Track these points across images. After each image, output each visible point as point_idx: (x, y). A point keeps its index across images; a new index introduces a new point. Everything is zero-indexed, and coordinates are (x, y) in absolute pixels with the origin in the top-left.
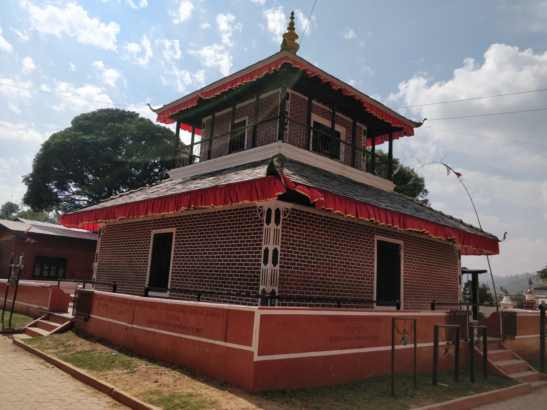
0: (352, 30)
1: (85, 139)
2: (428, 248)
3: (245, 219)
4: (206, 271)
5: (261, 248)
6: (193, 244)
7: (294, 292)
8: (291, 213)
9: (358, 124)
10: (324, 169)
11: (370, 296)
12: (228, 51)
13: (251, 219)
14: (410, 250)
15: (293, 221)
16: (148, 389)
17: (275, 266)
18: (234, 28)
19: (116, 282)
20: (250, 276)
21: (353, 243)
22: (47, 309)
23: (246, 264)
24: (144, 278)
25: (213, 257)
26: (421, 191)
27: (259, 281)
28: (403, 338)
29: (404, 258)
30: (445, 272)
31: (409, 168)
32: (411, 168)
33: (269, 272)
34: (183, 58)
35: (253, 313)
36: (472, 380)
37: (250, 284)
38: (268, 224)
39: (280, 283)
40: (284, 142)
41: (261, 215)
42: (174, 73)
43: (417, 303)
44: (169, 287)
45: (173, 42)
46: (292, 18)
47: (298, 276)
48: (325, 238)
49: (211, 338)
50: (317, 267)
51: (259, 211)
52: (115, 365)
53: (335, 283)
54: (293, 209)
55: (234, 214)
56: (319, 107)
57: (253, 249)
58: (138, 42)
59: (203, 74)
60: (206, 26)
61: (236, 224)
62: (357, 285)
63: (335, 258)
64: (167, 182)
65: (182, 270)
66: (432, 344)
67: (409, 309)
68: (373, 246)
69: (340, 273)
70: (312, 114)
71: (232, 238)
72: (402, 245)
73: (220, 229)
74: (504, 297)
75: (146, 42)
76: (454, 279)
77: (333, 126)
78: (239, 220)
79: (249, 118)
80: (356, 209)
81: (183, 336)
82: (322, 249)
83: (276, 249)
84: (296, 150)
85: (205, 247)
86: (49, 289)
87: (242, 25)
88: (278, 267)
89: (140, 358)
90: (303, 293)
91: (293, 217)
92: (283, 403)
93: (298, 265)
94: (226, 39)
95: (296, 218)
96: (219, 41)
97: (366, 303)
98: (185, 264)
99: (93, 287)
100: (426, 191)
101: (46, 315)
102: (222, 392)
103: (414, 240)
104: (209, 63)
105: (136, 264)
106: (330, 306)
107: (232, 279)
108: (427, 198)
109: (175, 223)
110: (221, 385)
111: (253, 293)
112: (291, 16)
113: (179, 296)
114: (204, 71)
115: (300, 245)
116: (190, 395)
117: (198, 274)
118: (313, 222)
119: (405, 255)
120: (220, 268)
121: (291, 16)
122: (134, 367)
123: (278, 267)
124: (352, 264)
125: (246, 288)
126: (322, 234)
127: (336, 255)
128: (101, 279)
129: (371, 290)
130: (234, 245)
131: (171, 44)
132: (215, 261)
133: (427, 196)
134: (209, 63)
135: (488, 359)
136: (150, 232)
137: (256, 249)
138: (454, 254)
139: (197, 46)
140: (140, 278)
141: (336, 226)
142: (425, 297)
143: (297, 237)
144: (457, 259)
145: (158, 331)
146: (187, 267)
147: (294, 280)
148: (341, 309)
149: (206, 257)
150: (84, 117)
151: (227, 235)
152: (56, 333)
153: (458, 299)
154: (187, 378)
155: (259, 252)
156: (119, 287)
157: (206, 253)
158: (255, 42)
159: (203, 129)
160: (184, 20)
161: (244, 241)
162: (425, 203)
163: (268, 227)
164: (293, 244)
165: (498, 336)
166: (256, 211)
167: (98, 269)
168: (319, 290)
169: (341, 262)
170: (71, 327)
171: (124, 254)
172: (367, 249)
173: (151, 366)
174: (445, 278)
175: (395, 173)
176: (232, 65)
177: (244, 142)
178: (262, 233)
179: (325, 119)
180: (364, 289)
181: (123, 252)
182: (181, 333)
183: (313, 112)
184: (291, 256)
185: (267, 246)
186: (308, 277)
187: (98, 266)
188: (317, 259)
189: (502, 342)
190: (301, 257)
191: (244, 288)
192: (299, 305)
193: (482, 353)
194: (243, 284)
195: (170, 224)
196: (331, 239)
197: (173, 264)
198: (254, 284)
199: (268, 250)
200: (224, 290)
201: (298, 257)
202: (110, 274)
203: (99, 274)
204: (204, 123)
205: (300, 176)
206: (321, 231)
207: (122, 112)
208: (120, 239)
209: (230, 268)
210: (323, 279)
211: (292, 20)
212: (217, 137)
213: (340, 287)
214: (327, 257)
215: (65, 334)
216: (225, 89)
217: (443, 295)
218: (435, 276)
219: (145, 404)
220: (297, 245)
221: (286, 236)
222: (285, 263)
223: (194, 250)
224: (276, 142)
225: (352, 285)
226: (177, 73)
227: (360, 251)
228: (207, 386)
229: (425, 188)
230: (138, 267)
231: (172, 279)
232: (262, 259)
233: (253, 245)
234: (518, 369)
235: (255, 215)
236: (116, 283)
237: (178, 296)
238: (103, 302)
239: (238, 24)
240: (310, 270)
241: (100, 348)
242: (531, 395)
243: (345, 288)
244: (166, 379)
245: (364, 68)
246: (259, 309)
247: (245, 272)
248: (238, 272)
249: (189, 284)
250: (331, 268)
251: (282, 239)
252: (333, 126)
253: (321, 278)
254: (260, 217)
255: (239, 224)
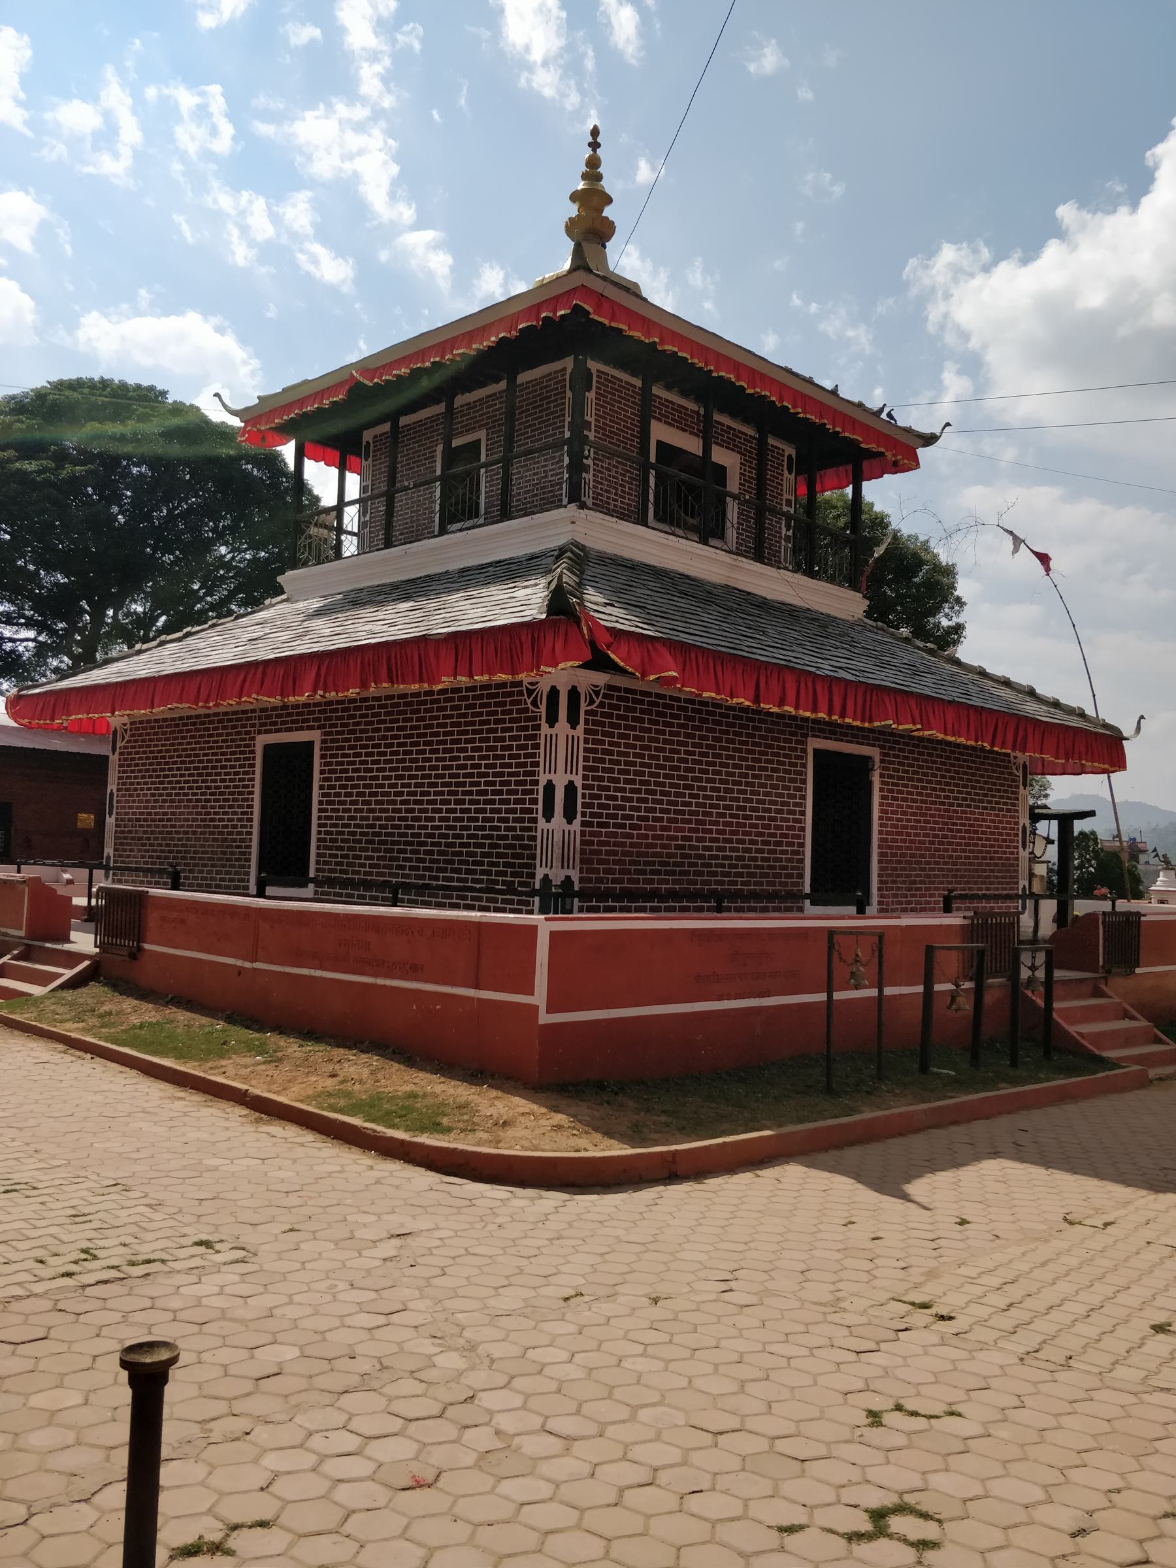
0: (773, 41)
1: (26, 473)
2: (942, 763)
3: (495, 713)
4: (405, 835)
5: (536, 783)
6: (367, 770)
7: (614, 881)
8: (605, 696)
9: (771, 441)
10: (686, 572)
11: (793, 884)
12: (382, 124)
13: (510, 712)
14: (897, 770)
15: (610, 716)
16: (319, 1089)
17: (570, 822)
18: (394, 41)
19: (178, 864)
20: (512, 846)
21: (754, 760)
22: (22, 933)
23: (501, 820)
24: (244, 853)
25: (420, 802)
26: (947, 601)
27: (534, 857)
28: (852, 973)
29: (881, 790)
30: (984, 820)
31: (917, 538)
32: (922, 538)
33: (558, 837)
34: (239, 148)
35: (533, 930)
36: (1014, 1064)
37: (512, 865)
38: (552, 726)
39: (582, 861)
40: (583, 506)
41: (535, 703)
42: (215, 201)
43: (913, 896)
44: (312, 874)
45: (202, 94)
46: (595, 145)
47: (623, 844)
48: (686, 753)
49: (445, 983)
50: (669, 820)
51: (530, 692)
52: (232, 1048)
53: (711, 857)
54: (610, 687)
55: (466, 698)
56: (671, 402)
57: (517, 783)
58: (92, 96)
59: (306, 206)
60: (306, 34)
61: (473, 723)
62: (763, 860)
63: (711, 798)
64: (281, 606)
65: (342, 833)
66: (920, 989)
67: (892, 910)
68: (804, 766)
69: (723, 832)
70: (653, 423)
71: (465, 758)
72: (877, 759)
73: (433, 734)
74: (1161, 874)
75: (115, 96)
76: (1008, 834)
77: (707, 450)
78: (480, 714)
79: (488, 434)
80: (758, 684)
81: (380, 981)
82: (680, 778)
83: (571, 783)
84: (615, 526)
85: (398, 777)
86: (21, 887)
87: (420, 30)
88: (577, 825)
89: (280, 1033)
90: (637, 881)
91: (611, 706)
92: (601, 1104)
93: (624, 817)
94: (370, 79)
95: (618, 708)
96: (348, 89)
97: (789, 901)
98: (351, 818)
99: (107, 877)
100: (958, 601)
101: (21, 948)
102: (474, 1089)
103: (908, 744)
104: (324, 167)
105: (221, 820)
106: (700, 909)
107: (469, 854)
108: (961, 620)
109: (317, 720)
110: (472, 1075)
111: (521, 884)
112: (590, 139)
113: (340, 895)
114: (308, 194)
115: (627, 772)
116: (412, 1095)
117: (384, 842)
118: (659, 714)
119: (883, 783)
120: (440, 828)
121: (590, 139)
122: (275, 1051)
123: (577, 825)
124: (752, 809)
125: (504, 874)
126: (679, 743)
127: (713, 789)
128: (129, 856)
129: (798, 868)
130: (471, 775)
131: (197, 100)
132: (425, 811)
133: (962, 614)
134: (324, 167)
135: (1055, 1015)
136: (253, 739)
137: (524, 783)
138: (1011, 774)
139: (281, 106)
140: (232, 853)
141: (715, 722)
142: (933, 883)
143: (620, 754)
144: (1017, 787)
145: (318, 973)
146: (357, 826)
147: (615, 853)
148: (724, 915)
149: (403, 802)
150: (12, 406)
151: (451, 751)
152: (62, 987)
153: (1017, 883)
154: (396, 1066)
155: (531, 792)
156: (186, 878)
157: (401, 794)
158: (465, 92)
159: (366, 460)
160: (233, 12)
161: (493, 766)
162: (957, 633)
163: (553, 731)
164: (612, 771)
165: (1092, 967)
166: (521, 693)
167: (116, 832)
168: (673, 873)
169: (726, 807)
170: (94, 973)
171: (186, 795)
172: (789, 772)
173: (309, 1047)
174: (984, 833)
175: (876, 555)
176: (395, 169)
177: (478, 504)
178: (537, 746)
179: (687, 434)
180: (782, 868)
181: (182, 788)
182: (376, 976)
183: (655, 418)
184: (608, 798)
185: (551, 777)
186: (648, 846)
187: (117, 826)
188: (669, 803)
189: (1103, 981)
190: (631, 800)
191: (498, 873)
192: (628, 910)
193: (1041, 1003)
194: (497, 865)
195: (304, 721)
196: (701, 754)
197: (320, 818)
198: (521, 866)
200: (451, 879)
201: (624, 799)
202: (151, 845)
203: (122, 844)
204: (368, 443)
205: (628, 605)
206: (678, 734)
207: (119, 387)
208: (171, 757)
209: (463, 828)
210: (682, 847)
211: (594, 151)
212: (407, 488)
213: (723, 866)
214: (691, 796)
215: (84, 990)
216: (423, 362)
217: (979, 877)
218: (959, 831)
219: (325, 1113)
220: (620, 772)
221: (595, 751)
222: (592, 815)
223: (369, 786)
224: (563, 510)
225: (751, 859)
226: (225, 201)
227: (770, 778)
228: (443, 1079)
229: (956, 593)
230: (226, 826)
231: (318, 855)
232: (540, 806)
233: (517, 774)
234: (1128, 1039)
235: (519, 702)
236: (179, 868)
237: (336, 894)
238: (175, 915)
239: (406, 28)
240: (653, 828)
241: (182, 1016)
242: (1142, 1093)
243: (736, 866)
244: (352, 1069)
245: (810, 177)
247: (500, 837)
248: (484, 837)
249: (363, 865)
250: (703, 822)
251: (586, 759)
252: (707, 450)
253: (678, 847)
254: (531, 708)
255: (482, 723)
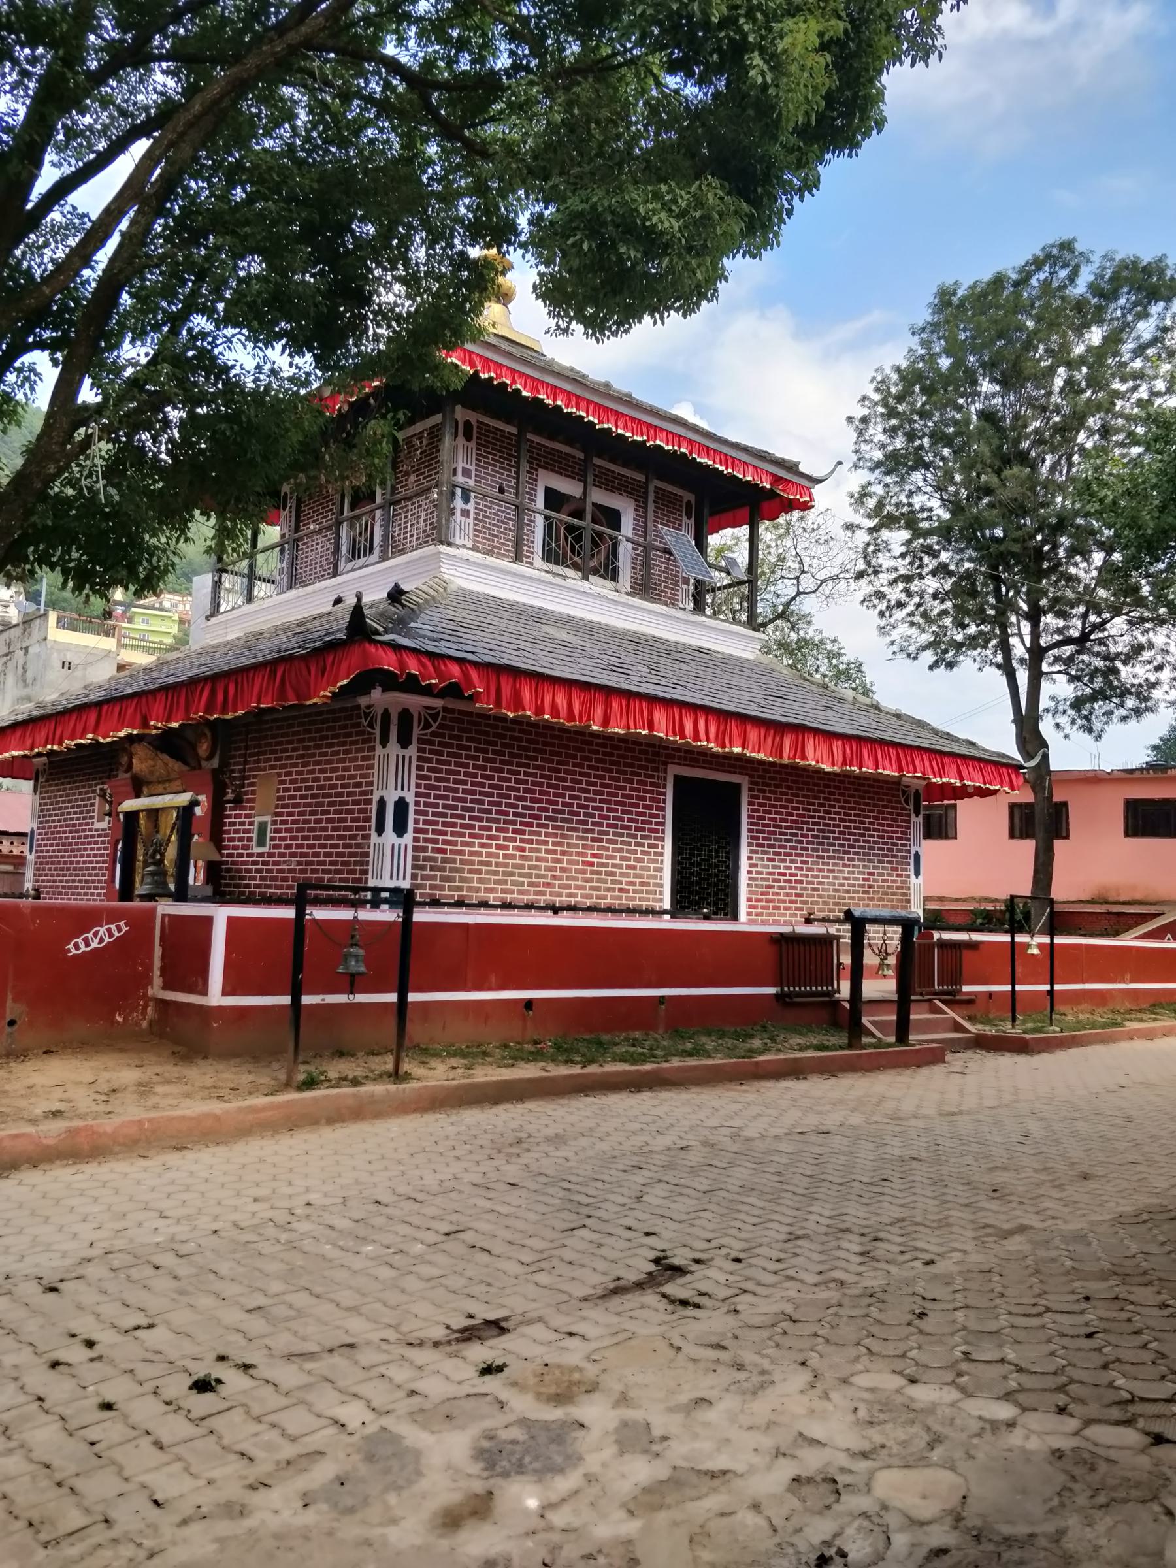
5: (369, 802)
38: (384, 746)
41: (371, 725)
54: (445, 709)
199: (407, 805)
246: (917, 874)
